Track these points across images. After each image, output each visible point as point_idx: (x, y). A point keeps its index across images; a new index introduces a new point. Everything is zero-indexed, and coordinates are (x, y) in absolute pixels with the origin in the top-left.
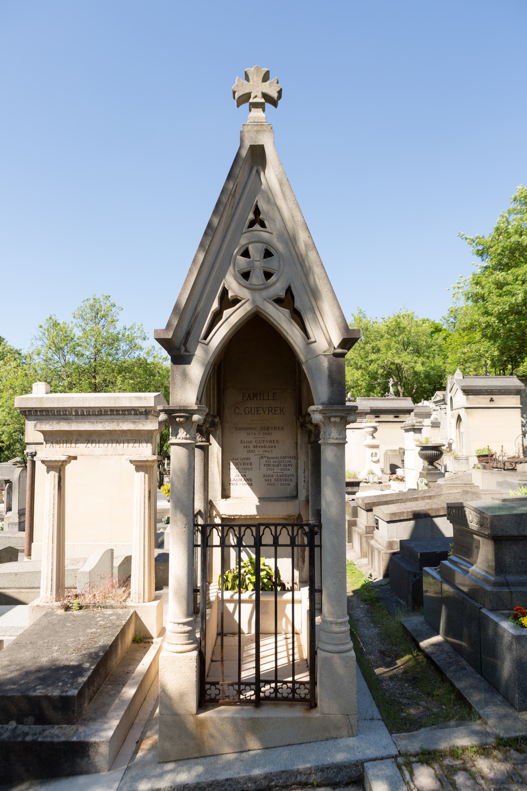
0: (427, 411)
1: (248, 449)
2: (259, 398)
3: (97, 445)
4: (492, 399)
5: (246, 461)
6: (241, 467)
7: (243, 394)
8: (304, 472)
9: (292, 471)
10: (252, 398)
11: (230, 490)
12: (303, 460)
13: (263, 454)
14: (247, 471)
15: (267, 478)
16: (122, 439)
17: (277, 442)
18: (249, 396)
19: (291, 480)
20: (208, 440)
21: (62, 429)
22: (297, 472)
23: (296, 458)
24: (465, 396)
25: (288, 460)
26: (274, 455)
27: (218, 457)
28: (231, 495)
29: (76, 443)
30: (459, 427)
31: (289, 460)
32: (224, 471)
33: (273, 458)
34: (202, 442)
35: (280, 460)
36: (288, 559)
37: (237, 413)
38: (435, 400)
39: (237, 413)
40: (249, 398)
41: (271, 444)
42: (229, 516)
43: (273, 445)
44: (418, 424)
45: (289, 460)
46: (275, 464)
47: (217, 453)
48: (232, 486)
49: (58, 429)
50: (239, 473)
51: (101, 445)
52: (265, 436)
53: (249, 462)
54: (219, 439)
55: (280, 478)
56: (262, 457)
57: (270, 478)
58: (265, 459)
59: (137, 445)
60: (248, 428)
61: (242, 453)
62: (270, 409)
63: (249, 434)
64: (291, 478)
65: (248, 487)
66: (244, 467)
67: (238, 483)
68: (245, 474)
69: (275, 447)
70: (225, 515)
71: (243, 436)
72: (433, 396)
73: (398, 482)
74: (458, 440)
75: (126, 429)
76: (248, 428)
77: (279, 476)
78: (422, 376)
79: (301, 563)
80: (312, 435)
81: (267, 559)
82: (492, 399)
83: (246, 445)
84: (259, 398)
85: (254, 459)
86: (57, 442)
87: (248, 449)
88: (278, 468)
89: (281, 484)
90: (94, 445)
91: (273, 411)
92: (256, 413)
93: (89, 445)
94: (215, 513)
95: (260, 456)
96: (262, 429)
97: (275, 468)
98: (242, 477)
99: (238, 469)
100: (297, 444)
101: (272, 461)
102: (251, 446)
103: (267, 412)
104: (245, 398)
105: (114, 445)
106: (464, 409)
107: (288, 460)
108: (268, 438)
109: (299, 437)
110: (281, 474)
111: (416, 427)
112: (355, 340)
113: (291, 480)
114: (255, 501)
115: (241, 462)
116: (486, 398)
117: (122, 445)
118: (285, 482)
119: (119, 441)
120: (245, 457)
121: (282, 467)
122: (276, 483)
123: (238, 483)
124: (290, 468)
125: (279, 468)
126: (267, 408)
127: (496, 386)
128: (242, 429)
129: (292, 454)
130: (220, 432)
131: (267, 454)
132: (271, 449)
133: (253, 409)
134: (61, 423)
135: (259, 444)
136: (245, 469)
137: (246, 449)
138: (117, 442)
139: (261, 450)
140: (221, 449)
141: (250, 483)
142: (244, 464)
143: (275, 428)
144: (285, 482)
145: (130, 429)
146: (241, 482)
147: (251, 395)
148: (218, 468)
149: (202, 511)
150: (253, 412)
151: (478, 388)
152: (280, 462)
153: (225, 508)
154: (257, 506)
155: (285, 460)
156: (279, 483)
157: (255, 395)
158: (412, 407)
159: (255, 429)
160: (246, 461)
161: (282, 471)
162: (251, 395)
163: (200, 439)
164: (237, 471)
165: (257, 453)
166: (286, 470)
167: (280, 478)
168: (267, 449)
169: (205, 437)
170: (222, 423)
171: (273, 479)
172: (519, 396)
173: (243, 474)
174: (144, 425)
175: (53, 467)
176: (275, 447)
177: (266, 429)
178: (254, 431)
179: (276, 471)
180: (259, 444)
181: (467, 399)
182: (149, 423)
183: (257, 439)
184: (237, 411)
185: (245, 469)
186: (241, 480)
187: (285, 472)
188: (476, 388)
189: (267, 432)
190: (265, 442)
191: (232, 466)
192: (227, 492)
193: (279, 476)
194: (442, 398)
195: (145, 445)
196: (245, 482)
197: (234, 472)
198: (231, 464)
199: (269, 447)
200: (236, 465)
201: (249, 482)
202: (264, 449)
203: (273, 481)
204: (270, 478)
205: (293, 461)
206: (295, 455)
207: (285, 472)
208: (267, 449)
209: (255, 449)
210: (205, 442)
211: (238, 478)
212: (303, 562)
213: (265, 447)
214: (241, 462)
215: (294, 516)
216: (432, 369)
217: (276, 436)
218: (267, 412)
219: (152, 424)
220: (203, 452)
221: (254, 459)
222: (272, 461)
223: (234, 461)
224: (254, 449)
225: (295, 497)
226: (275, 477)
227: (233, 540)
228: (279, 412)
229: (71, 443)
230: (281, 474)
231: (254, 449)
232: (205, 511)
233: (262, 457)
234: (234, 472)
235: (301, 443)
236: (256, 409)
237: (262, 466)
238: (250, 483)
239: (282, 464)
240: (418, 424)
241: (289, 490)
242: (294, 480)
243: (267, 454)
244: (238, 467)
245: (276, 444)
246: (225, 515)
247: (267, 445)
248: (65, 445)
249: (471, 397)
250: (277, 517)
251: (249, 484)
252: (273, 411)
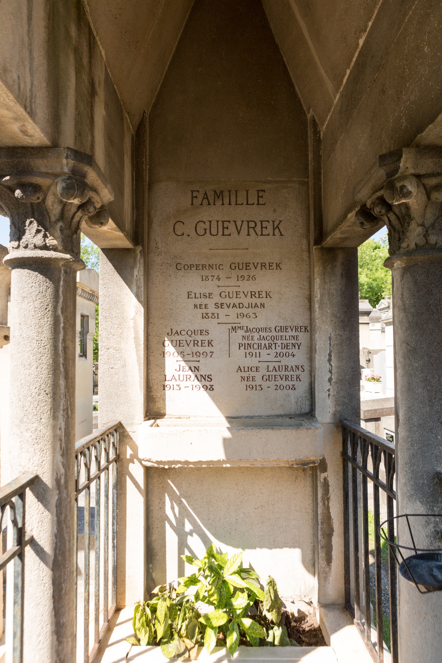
0: (377, 316)
1: (204, 311)
2: (226, 201)
5: (199, 338)
6: (188, 350)
7: (192, 192)
8: (330, 360)
9: (300, 358)
10: (212, 202)
11: (164, 400)
12: (325, 331)
13: (237, 321)
14: (201, 358)
15: (246, 375)
17: (268, 295)
18: (206, 196)
19: (298, 377)
20: (71, 245)
22: (311, 359)
23: (310, 329)
25: (290, 333)
26: (260, 323)
27: (136, 332)
28: (168, 411)
31: (294, 333)
32: (151, 358)
33: (259, 330)
34: (45, 247)
35: (275, 334)
36: (292, 550)
37: (179, 233)
38: (380, 308)
39: (179, 233)
40: (205, 201)
41: (254, 301)
42: (157, 462)
43: (259, 301)
45: (294, 333)
46: (263, 342)
47: (134, 319)
48: (168, 393)
50: (183, 364)
52: (240, 283)
53: (206, 338)
54: (138, 287)
55: (274, 373)
56: (234, 329)
57: (252, 374)
58: (241, 333)
60: (204, 266)
61: (189, 319)
62: (252, 225)
63: (205, 279)
64: (298, 373)
65: (204, 394)
66: (195, 349)
67: (183, 384)
68: (196, 364)
69: (263, 305)
70: (149, 461)
71: (193, 282)
72: (378, 304)
73: (375, 382)
76: (204, 266)
77: (271, 368)
78: (366, 287)
79: (322, 563)
80: (413, 225)
81: (247, 551)
83: (198, 302)
84: (226, 201)
85: (217, 332)
87: (204, 311)
88: (269, 351)
89: (277, 388)
91: (258, 229)
92: (220, 233)
94: (129, 452)
95: (229, 326)
96: (234, 266)
97: (264, 352)
98: (190, 373)
99: (181, 353)
100: (310, 299)
101: (256, 336)
102: (211, 303)
103: (244, 231)
104: (197, 202)
107: (290, 333)
108: (247, 286)
109: (317, 282)
110: (276, 365)
113: (298, 377)
114: (221, 428)
115: (189, 339)
118: (284, 383)
120: (197, 327)
122: (265, 384)
123: (183, 384)
124: (295, 351)
125: (273, 352)
126: (245, 224)
128: (191, 267)
129: (301, 320)
130: (142, 273)
131: (244, 322)
132: (254, 310)
133: (214, 224)
135: (227, 301)
136: (198, 354)
137: (199, 312)
139: (233, 312)
140: (142, 310)
141: (208, 384)
142: (196, 343)
143: (263, 265)
144: (284, 383)
146: (189, 383)
147: (211, 195)
148: (137, 351)
149: (47, 479)
150: (214, 231)
152: (274, 338)
153: (151, 444)
154: (225, 440)
155: (284, 334)
156: (272, 384)
157: (219, 195)
158: (370, 309)
159: (219, 267)
160: (199, 338)
161: (279, 359)
162: (211, 195)
163: (39, 240)
164: (180, 358)
165: (222, 319)
166: (287, 355)
167: (274, 373)
168: (244, 311)
169: (58, 233)
170: (146, 254)
171: (258, 376)
173: (193, 364)
176: (263, 305)
177: (243, 268)
178: (216, 272)
179: (264, 357)
180: (227, 301)
183: (223, 289)
184: (180, 229)
185: (198, 354)
186: (188, 378)
187: (285, 361)
189: (245, 273)
190: (242, 295)
191: (169, 348)
192: (159, 405)
193: (271, 368)
194: (387, 306)
196: (196, 382)
197: (173, 362)
198: (167, 343)
199: (250, 306)
200: (178, 344)
201: (207, 382)
202: (239, 311)
203: (259, 381)
204: (252, 374)
205: (303, 337)
206: (307, 323)
207: (285, 361)
208: (244, 311)
209: (219, 311)
210: (55, 249)
211: (181, 373)
212: (329, 560)
213: (241, 305)
214: (189, 339)
215: (314, 462)
216: (375, 280)
217: (266, 281)
218: (244, 231)
220: (49, 283)
221: (217, 332)
222: (256, 336)
223: (173, 338)
224: (216, 311)
225: (307, 415)
226: (262, 371)
227: (173, 508)
228: (270, 230)
230: (276, 365)
231: (216, 311)
232: (57, 481)
233: (234, 329)
234: (173, 362)
235: (322, 295)
236: (220, 224)
237: (234, 347)
238: (208, 384)
239: (279, 342)
241: (295, 399)
242: (305, 377)
243: (244, 322)
244: (181, 349)
245: (264, 300)
246: (149, 461)
247: (246, 301)
250: (274, 464)
251: (206, 388)
252: (258, 229)
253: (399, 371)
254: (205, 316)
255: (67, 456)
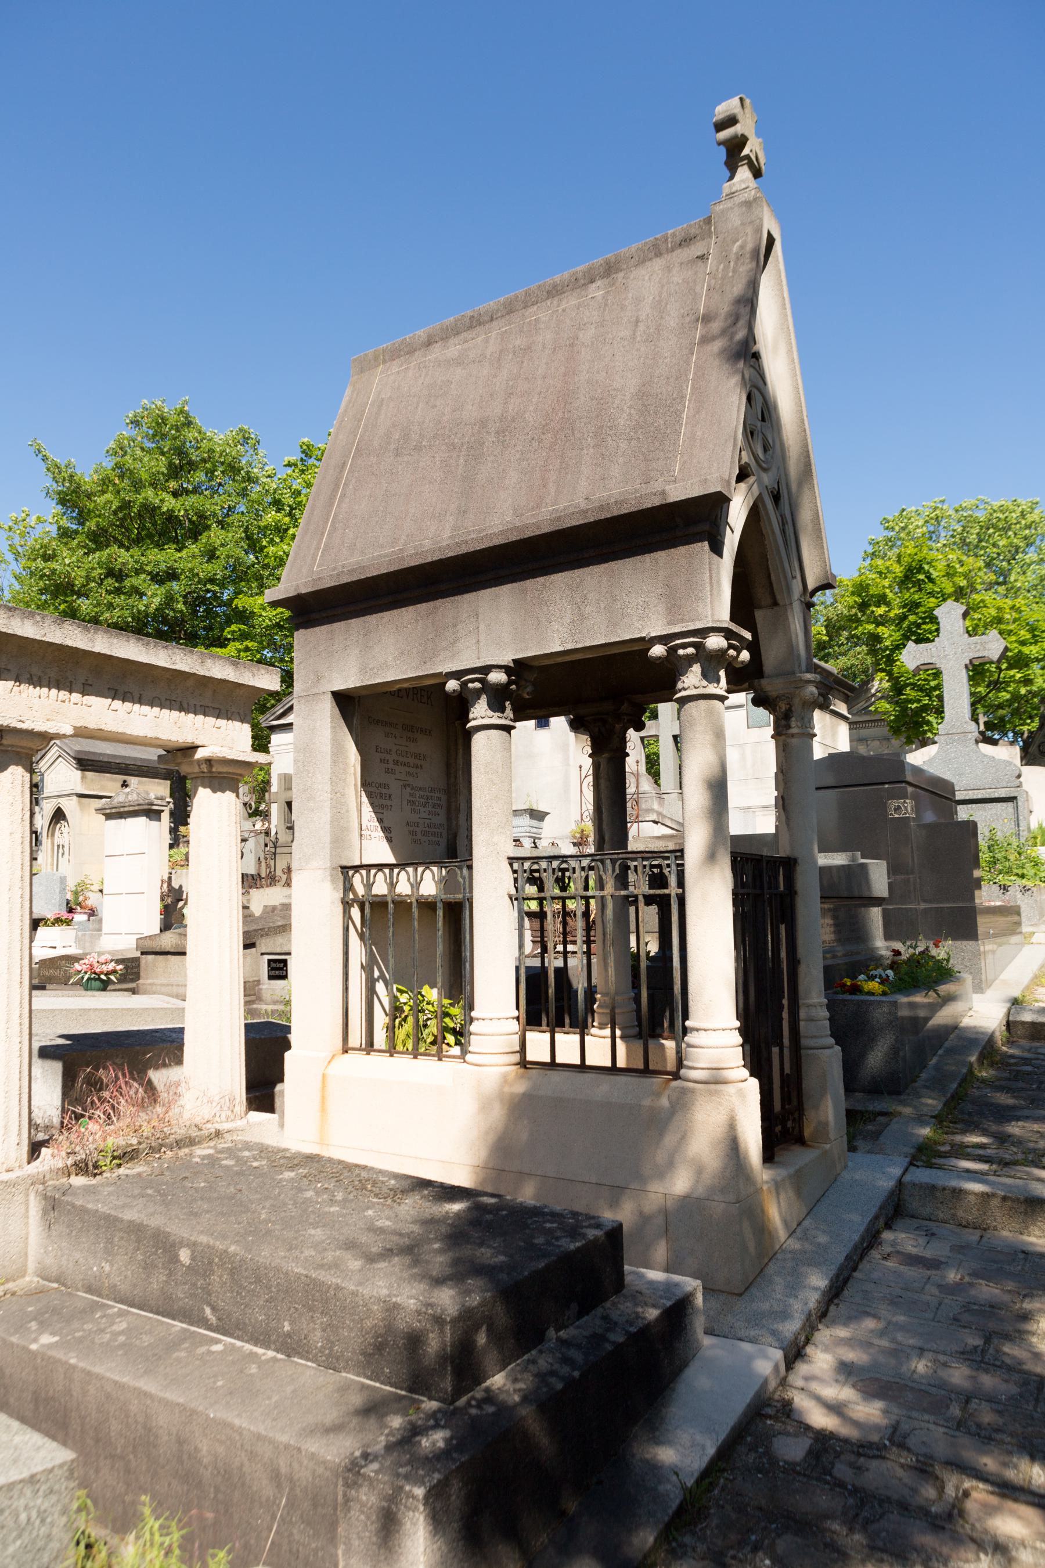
3: (137, 706)
4: (125, 781)
5: (384, 791)
16: (192, 702)
21: (70, 643)
24: (79, 772)
27: (355, 774)
29: (84, 693)
30: (53, 835)
44: (159, 802)
47: (354, 766)
49: (58, 641)
50: (373, 815)
51: (146, 709)
58: (408, 790)
59: (222, 722)
73: (63, 927)
74: (50, 860)
75: (219, 677)
76: (386, 723)
82: (125, 781)
85: (395, 788)
86: (36, 681)
90: (128, 705)
93: (117, 704)
97: (422, 809)
99: (372, 804)
102: (391, 758)
105: (175, 714)
106: (75, 797)
111: (154, 807)
112: (834, 587)
116: (115, 780)
117: (191, 716)
119: (185, 706)
121: (430, 809)
127: (136, 759)
131: (411, 780)
134: (66, 625)
135: (401, 759)
138: (181, 709)
145: (228, 678)
146: (374, 834)
151: (106, 759)
160: (384, 791)
172: (169, 782)
173: (381, 816)
174: (254, 675)
175: (18, 753)
180: (401, 759)
181: (83, 778)
182: (263, 672)
188: (101, 759)
195: (238, 724)
196: (382, 834)
202: (407, 769)
219: (267, 677)
221: (395, 788)
229: (71, 692)
237: (405, 803)
240: (159, 802)
243: (411, 780)
247: (412, 761)
248: (54, 691)
249: (89, 774)
253: (602, 782)
254: (387, 771)
255: (916, 1468)
